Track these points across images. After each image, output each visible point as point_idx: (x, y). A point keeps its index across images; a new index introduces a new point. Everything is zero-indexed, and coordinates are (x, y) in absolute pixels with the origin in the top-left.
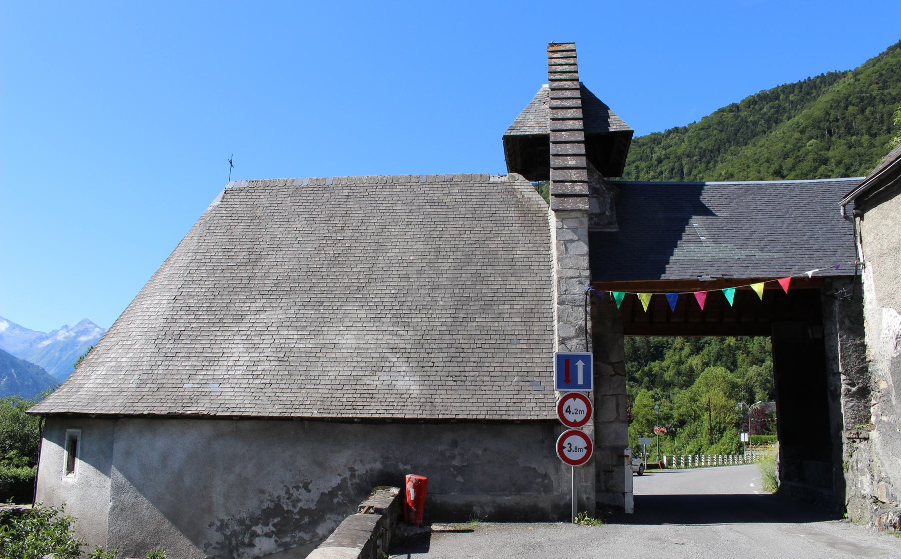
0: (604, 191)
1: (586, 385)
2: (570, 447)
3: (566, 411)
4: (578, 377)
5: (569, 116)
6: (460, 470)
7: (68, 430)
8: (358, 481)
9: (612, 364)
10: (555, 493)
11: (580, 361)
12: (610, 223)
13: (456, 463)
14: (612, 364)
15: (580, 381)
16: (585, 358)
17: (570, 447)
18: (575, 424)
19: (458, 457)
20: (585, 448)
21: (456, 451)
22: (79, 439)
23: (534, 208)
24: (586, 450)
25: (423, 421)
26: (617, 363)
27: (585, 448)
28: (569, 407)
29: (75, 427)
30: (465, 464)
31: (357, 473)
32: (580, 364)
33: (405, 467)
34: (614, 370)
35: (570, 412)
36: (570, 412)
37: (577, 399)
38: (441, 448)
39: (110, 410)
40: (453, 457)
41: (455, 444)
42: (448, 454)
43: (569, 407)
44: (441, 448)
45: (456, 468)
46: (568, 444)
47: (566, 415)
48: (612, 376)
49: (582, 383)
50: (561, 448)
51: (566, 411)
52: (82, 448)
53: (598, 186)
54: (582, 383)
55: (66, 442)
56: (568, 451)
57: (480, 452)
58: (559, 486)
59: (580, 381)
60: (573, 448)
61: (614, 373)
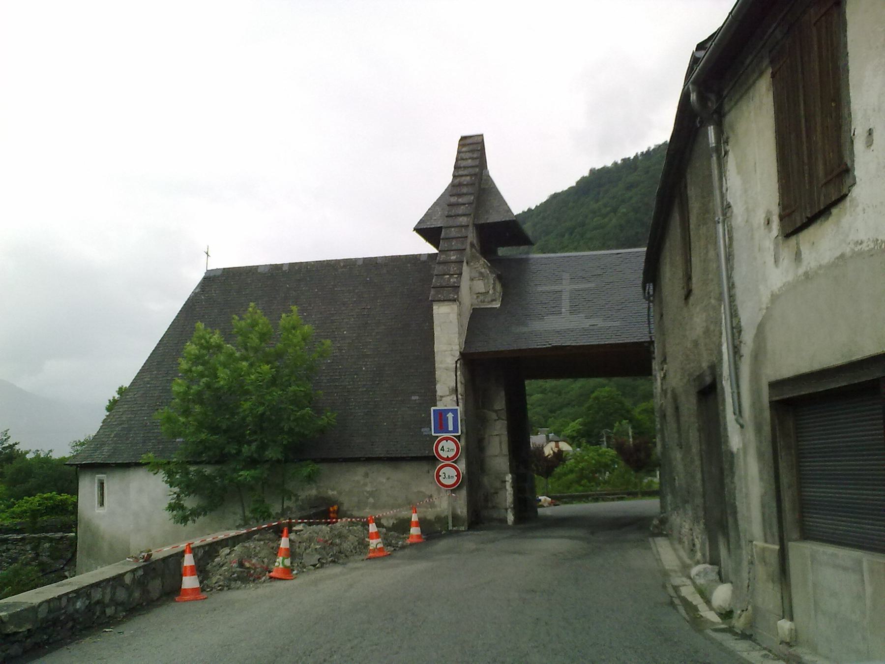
0: (488, 274)
1: (455, 430)
2: (445, 476)
3: (441, 450)
4: (449, 424)
5: (460, 212)
6: (372, 494)
7: (97, 476)
8: (301, 503)
9: (496, 411)
10: (439, 509)
11: (450, 413)
12: (493, 300)
13: (368, 489)
14: (496, 411)
15: (451, 428)
16: (454, 412)
17: (445, 476)
18: (448, 459)
19: (369, 484)
20: (456, 476)
21: (368, 480)
22: (105, 482)
23: (99, 567)
24: (440, 474)
25: (385, 459)
26: (499, 410)
27: (456, 476)
28: (443, 447)
29: (102, 473)
30: (374, 489)
31: (300, 498)
32: (450, 416)
33: (333, 493)
34: (497, 416)
35: (444, 450)
36: (444, 450)
37: (449, 441)
38: (356, 478)
39: (124, 460)
40: (365, 485)
41: (366, 475)
42: (362, 482)
43: (443, 447)
44: (356, 478)
45: (368, 492)
46: (444, 473)
47: (441, 452)
48: (495, 420)
49: (452, 429)
50: (438, 476)
51: (441, 450)
52: (108, 488)
53: (483, 270)
54: (452, 429)
55: (96, 485)
56: (444, 478)
57: (384, 481)
58: (179, 463)
59: (451, 428)
60: (447, 476)
61: (497, 418)
